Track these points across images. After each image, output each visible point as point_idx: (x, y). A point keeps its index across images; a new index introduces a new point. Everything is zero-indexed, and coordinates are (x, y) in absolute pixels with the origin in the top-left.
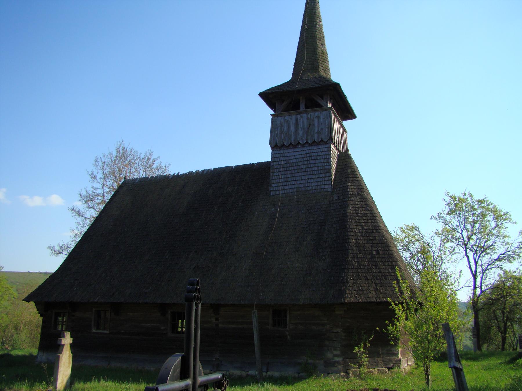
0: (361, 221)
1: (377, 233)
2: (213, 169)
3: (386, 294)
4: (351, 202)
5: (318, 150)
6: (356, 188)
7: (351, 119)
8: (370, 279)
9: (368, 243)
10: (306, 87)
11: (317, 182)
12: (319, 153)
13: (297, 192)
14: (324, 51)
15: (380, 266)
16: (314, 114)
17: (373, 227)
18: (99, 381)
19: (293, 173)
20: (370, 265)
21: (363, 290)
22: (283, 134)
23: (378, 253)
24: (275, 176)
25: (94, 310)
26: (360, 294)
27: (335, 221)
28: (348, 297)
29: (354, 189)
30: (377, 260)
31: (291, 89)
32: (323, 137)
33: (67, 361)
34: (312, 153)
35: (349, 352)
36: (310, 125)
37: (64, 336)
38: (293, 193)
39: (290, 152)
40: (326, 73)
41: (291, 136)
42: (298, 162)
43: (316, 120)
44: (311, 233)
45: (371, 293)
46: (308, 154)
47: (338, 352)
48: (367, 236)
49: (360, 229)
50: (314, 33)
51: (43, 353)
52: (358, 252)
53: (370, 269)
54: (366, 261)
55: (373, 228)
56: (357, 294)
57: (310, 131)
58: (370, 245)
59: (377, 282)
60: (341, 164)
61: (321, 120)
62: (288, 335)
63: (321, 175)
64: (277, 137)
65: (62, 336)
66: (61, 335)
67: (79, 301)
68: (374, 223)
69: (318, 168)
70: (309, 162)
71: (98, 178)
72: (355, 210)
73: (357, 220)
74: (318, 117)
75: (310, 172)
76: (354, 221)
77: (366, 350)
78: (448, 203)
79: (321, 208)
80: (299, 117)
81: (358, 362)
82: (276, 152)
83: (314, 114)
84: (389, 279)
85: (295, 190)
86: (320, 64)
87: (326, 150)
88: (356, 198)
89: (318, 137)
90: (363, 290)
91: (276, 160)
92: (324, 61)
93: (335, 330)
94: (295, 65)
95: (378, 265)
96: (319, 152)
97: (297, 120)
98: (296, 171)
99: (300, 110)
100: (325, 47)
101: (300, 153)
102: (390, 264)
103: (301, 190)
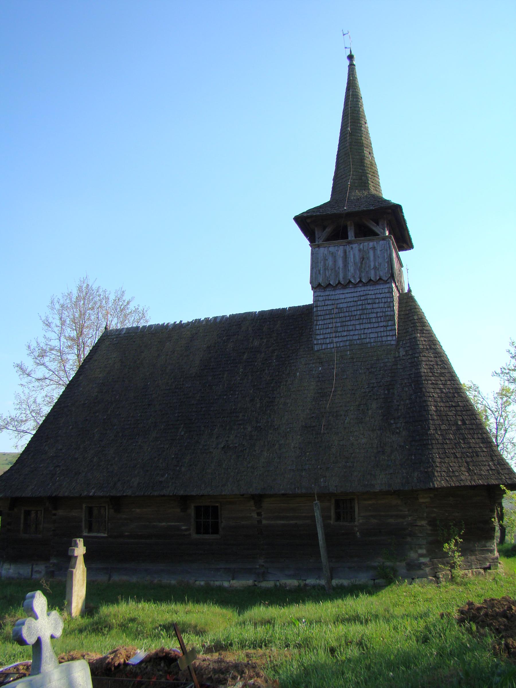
0: (439, 383)
1: (459, 398)
2: (228, 316)
3: (481, 475)
4: (424, 359)
5: (376, 292)
6: (426, 340)
7: (406, 250)
8: (460, 456)
9: (451, 411)
10: (357, 209)
11: (376, 332)
12: (377, 295)
13: (350, 345)
14: (373, 162)
15: (468, 439)
16: (368, 244)
17: (454, 390)
18: (176, 604)
19: (344, 322)
20: (457, 438)
21: (453, 472)
22: (328, 270)
23: (464, 423)
24: (319, 325)
25: (84, 506)
26: (450, 477)
27: (405, 383)
28: (437, 480)
29: (425, 341)
30: (464, 432)
31: (338, 212)
32: (381, 273)
33: (81, 577)
34: (369, 294)
35: (437, 550)
36: (363, 258)
37: (76, 545)
38: (345, 347)
39: (339, 294)
40: (377, 191)
41: (339, 273)
42: (350, 307)
43: (371, 253)
44: (377, 399)
45: (463, 474)
46: (363, 296)
47: (423, 551)
48: (448, 402)
49: (439, 393)
50: (359, 138)
51: (10, 565)
52: (441, 423)
53: (457, 444)
54: (451, 434)
55: (454, 392)
56: (447, 476)
57: (363, 266)
58: (453, 413)
59: (468, 460)
60: (404, 309)
61: (379, 252)
62: (357, 531)
63: (382, 324)
64: (320, 274)
65: (73, 544)
66: (71, 544)
67: (66, 494)
68: (454, 384)
69: (377, 315)
70: (364, 307)
71: (53, 325)
72: (430, 368)
73: (434, 382)
74: (374, 248)
75: (366, 320)
76: (431, 383)
77: (457, 547)
78: (514, 356)
79: (385, 366)
80: (348, 248)
81: (448, 563)
82: (319, 294)
83: (368, 244)
84: (481, 456)
85: (348, 343)
86: (370, 179)
87: (386, 292)
88: (429, 353)
89: (375, 275)
90: (453, 472)
91: (319, 303)
92: (374, 174)
93: (419, 523)
94: (335, 179)
95: (466, 438)
96: (377, 294)
97: (345, 252)
98: (348, 319)
99: (348, 239)
100: (373, 157)
101: (352, 295)
102: (480, 437)
103: (355, 343)
